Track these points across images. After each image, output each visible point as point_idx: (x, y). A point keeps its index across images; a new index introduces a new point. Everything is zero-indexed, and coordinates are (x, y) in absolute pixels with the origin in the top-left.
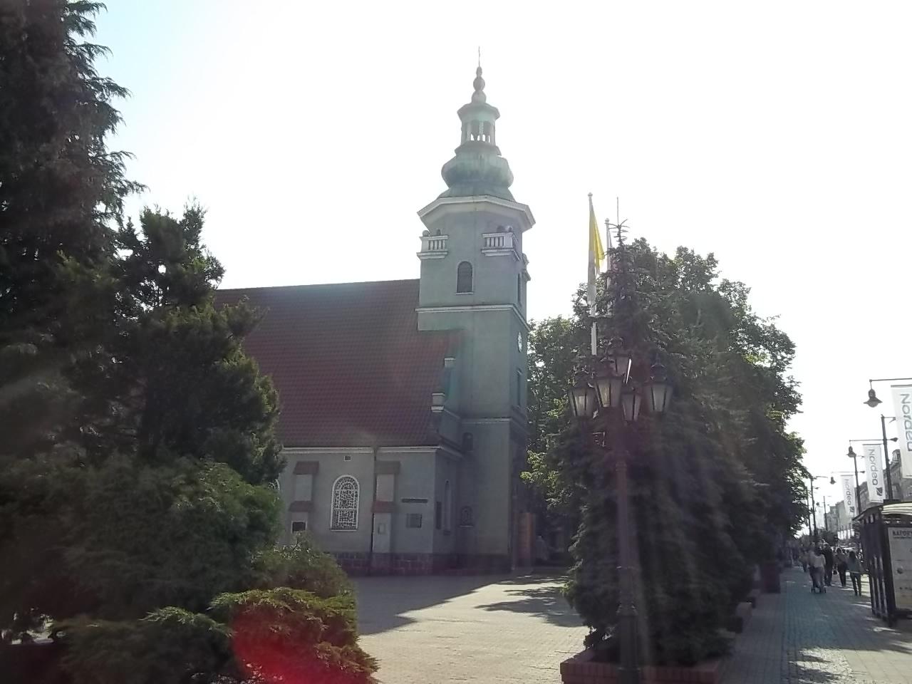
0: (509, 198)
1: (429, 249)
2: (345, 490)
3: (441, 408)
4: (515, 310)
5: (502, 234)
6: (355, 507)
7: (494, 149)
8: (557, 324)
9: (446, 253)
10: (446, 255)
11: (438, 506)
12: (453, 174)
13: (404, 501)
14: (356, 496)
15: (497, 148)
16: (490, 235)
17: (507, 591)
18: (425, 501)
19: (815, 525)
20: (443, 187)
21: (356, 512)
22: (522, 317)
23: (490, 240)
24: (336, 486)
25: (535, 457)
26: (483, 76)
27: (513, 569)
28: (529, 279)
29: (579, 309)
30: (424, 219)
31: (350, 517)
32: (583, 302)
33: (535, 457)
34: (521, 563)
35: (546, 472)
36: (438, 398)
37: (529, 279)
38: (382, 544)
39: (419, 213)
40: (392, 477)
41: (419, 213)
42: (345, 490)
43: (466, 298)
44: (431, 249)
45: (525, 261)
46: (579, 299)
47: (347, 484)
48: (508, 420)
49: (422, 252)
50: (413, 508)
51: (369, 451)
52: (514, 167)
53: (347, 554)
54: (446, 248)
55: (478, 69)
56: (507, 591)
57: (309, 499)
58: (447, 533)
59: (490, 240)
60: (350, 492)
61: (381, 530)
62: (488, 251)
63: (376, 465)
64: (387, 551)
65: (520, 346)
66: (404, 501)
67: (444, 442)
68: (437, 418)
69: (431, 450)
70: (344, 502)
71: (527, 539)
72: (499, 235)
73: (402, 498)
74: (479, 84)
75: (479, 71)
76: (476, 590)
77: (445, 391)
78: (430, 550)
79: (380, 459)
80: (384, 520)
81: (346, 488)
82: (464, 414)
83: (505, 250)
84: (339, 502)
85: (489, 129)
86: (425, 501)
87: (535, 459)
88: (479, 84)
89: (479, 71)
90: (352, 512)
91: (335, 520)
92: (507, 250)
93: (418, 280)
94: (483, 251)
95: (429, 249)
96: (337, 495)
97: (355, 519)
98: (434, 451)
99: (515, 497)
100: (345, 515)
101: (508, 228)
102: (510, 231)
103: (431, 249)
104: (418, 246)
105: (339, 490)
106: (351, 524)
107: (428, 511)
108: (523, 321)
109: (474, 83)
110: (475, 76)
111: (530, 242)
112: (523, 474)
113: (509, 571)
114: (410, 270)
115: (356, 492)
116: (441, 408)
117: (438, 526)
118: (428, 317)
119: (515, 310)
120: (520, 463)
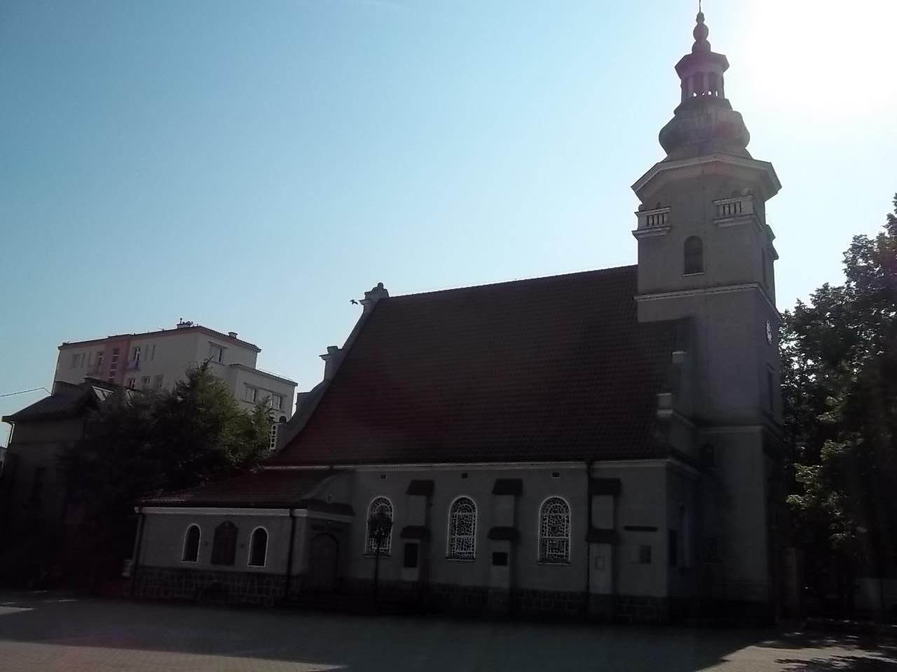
0: (747, 156)
1: (648, 224)
3: (670, 412)
5: (740, 199)
6: (567, 535)
7: (726, 104)
8: (825, 296)
9: (668, 228)
10: (669, 231)
11: (673, 537)
12: (669, 137)
13: (628, 528)
14: (568, 521)
15: (727, 101)
16: (723, 202)
17: (781, 661)
20: (661, 155)
21: (567, 541)
22: (770, 300)
23: (653, 218)
24: (543, 509)
25: (806, 472)
26: (705, 23)
28: (777, 257)
29: (852, 272)
30: (639, 194)
32: (861, 262)
33: (806, 472)
35: (822, 495)
36: (665, 397)
37: (777, 257)
38: (601, 583)
39: (634, 187)
40: (610, 498)
41: (634, 187)
42: (554, 515)
44: (650, 226)
45: (770, 236)
46: (854, 258)
49: (638, 230)
51: (582, 466)
52: (711, 43)
54: (668, 221)
55: (698, 16)
56: (781, 661)
57: (510, 524)
59: (653, 218)
60: (560, 517)
62: (721, 221)
64: (608, 591)
66: (628, 528)
67: (674, 453)
68: (666, 425)
69: (659, 464)
70: (554, 528)
72: (734, 200)
74: (700, 32)
75: (700, 17)
76: (727, 658)
79: (597, 475)
80: (602, 552)
81: (555, 512)
82: (700, 422)
83: (745, 217)
85: (717, 84)
86: (654, 529)
87: (807, 475)
88: (700, 32)
89: (700, 17)
90: (563, 542)
92: (748, 217)
93: (635, 266)
94: (715, 222)
95: (718, 214)
97: (567, 550)
100: (555, 544)
101: (745, 191)
102: (749, 193)
103: (650, 226)
104: (634, 224)
106: (562, 556)
107: (658, 542)
108: (771, 305)
109: (740, 114)
110: (696, 24)
111: (775, 212)
112: (792, 498)
114: (625, 254)
115: (568, 517)
116: (670, 412)
118: (650, 308)
119: (761, 290)
120: (781, 482)
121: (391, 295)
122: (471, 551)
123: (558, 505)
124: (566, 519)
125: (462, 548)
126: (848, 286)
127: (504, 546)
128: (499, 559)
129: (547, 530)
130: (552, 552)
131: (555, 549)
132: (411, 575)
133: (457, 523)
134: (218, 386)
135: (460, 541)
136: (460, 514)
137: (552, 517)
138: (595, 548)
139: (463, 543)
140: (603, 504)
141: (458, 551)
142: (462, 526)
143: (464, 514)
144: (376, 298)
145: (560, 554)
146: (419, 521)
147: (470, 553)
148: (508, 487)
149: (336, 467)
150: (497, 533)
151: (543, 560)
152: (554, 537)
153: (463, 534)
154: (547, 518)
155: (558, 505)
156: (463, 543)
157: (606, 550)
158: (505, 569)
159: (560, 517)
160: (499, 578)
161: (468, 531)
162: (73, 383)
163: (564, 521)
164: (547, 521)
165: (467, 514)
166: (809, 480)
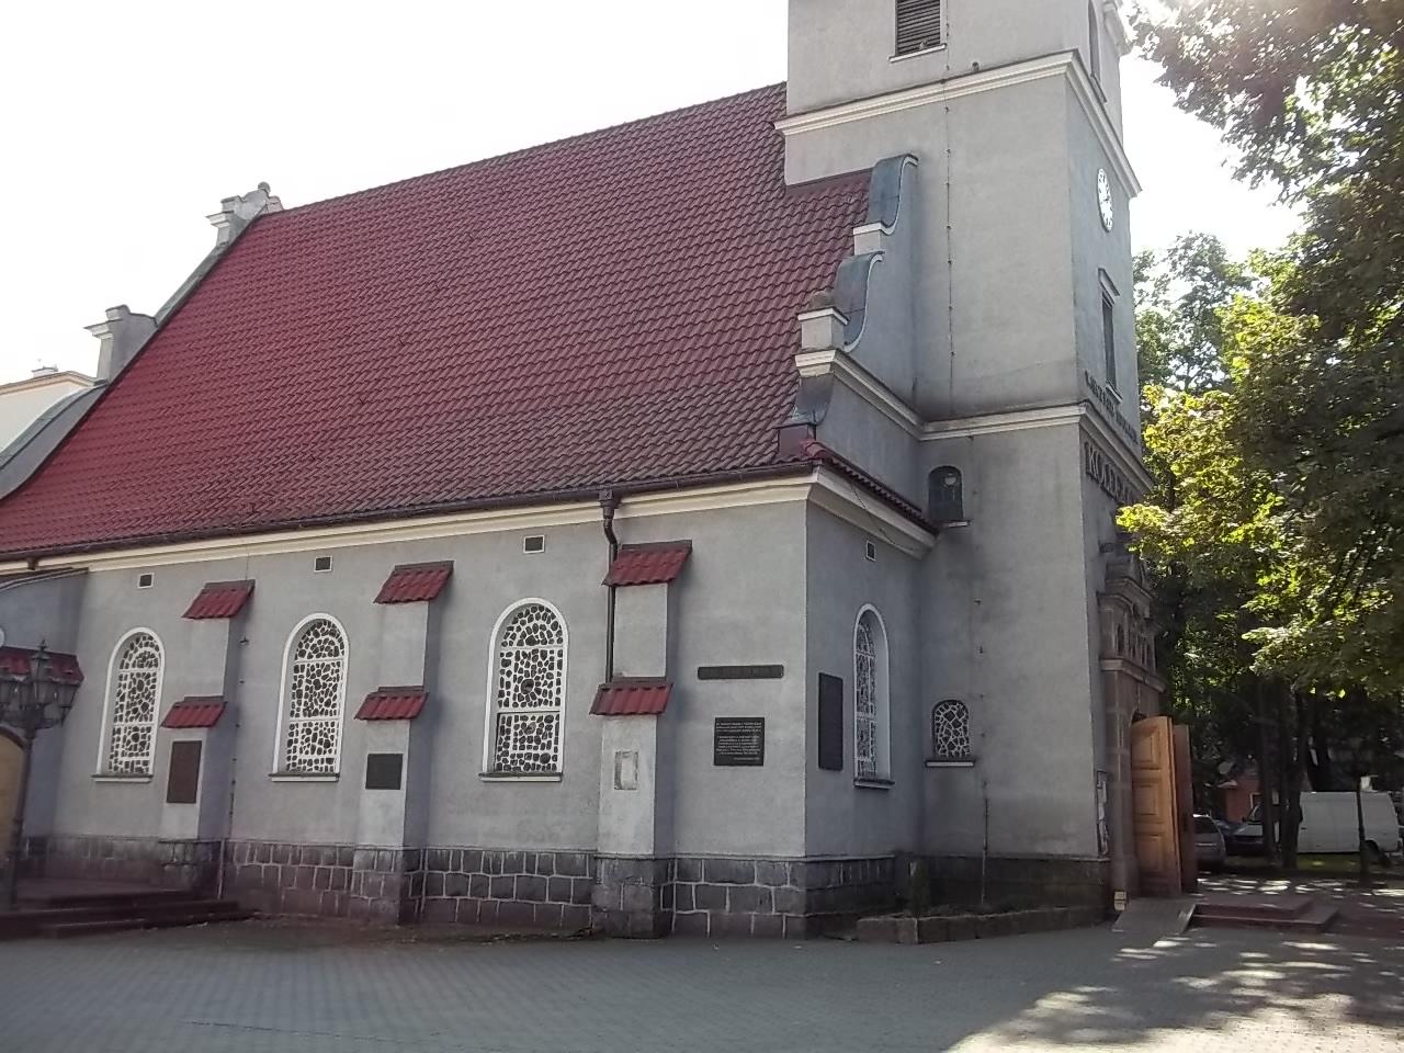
2: (528, 649)
4: (1095, 421)
6: (558, 703)
11: (829, 695)
13: (705, 673)
14: (560, 664)
18: (774, 672)
19: (631, 503)
27: (1119, 907)
31: (545, 736)
34: (1146, 885)
42: (528, 649)
43: (924, 63)
47: (536, 628)
48: (1075, 410)
50: (738, 699)
51: (592, 514)
53: (531, 857)
57: (417, 680)
58: (871, 785)
60: (544, 655)
61: (626, 778)
63: (615, 555)
64: (645, 849)
65: (1106, 209)
66: (705, 673)
69: (792, 493)
71: (1162, 802)
73: (369, 752)
77: (851, 316)
78: (793, 846)
81: (531, 642)
84: (513, 685)
86: (774, 672)
90: (549, 719)
91: (500, 746)
96: (506, 663)
98: (803, 495)
99: (1114, 665)
105: (514, 649)
106: (545, 759)
113: (1109, 915)
117: (829, 753)
119: (1095, 421)
121: (287, 207)
124: (557, 659)
125: (313, 749)
127: (395, 738)
128: (382, 772)
129: (512, 690)
130: (522, 748)
131: (530, 740)
132: (182, 823)
133: (304, 684)
135: (309, 732)
136: (314, 661)
137: (524, 654)
138: (614, 729)
139: (315, 735)
140: (645, 607)
141: (303, 757)
142: (314, 691)
143: (321, 660)
144: (249, 212)
145: (540, 752)
146: (210, 683)
149: (42, 563)
150: (380, 706)
151: (496, 771)
152: (527, 708)
154: (513, 658)
155: (540, 622)
157: (642, 734)
161: (327, 704)
162: (424, 656)
163: (552, 668)
164: (511, 668)
165: (328, 660)
166: (1199, 428)
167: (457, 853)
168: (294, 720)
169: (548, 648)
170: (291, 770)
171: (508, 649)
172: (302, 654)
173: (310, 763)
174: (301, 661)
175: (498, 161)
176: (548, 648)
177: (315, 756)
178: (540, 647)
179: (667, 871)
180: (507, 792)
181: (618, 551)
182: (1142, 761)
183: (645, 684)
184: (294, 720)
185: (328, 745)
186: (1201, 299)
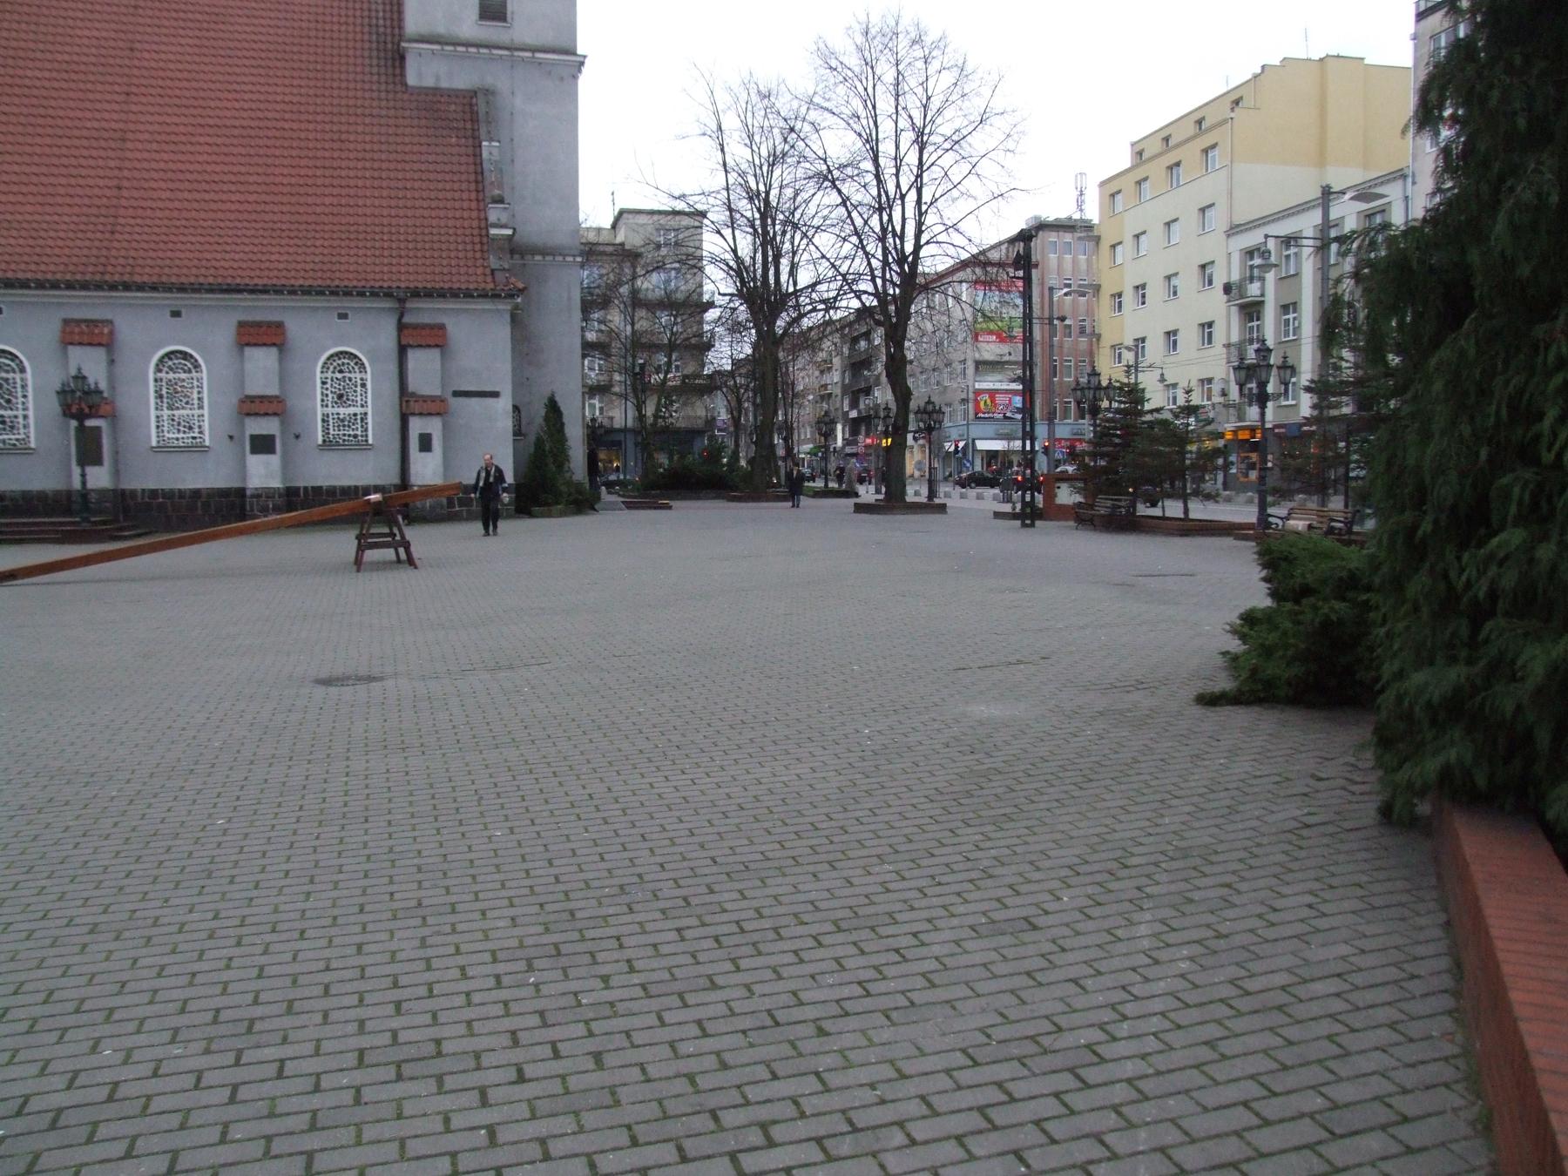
2: (339, 376)
13: (457, 394)
18: (495, 395)
40: (436, 353)
43: (490, 32)
57: (273, 391)
66: (457, 394)
70: (340, 396)
81: (341, 371)
86: (495, 395)
91: (326, 430)
100: (343, 421)
105: (329, 375)
122: (196, 435)
123: (346, 361)
126: (1021, 486)
128: (263, 445)
134: (1216, 388)
136: (171, 375)
141: (171, 435)
143: (177, 376)
147: (194, 438)
148: (82, 333)
150: (253, 406)
153: (178, 408)
156: (179, 424)
158: (274, 460)
159: (350, 379)
160: (263, 473)
161: (187, 403)
167: (306, 488)
168: (159, 413)
169: (352, 375)
170: (163, 449)
171: (325, 375)
172: (160, 371)
173: (177, 439)
174: (159, 375)
175: (577, 136)
176: (352, 375)
177: (181, 435)
178: (348, 375)
179: (363, 522)
180: (332, 457)
181: (401, 327)
182: (495, 527)
183: (433, 399)
184: (159, 413)
185: (190, 428)
186: (1337, 239)
